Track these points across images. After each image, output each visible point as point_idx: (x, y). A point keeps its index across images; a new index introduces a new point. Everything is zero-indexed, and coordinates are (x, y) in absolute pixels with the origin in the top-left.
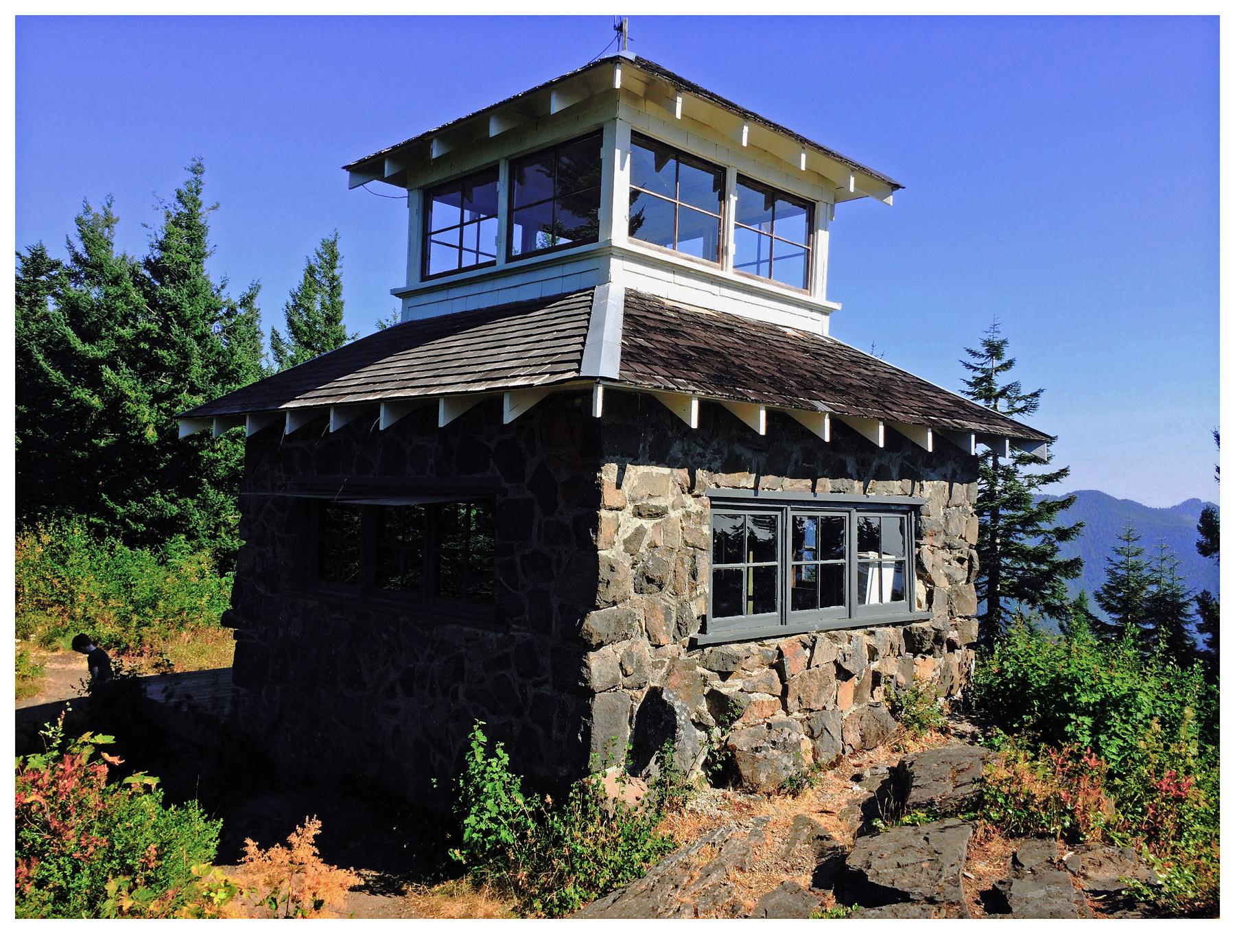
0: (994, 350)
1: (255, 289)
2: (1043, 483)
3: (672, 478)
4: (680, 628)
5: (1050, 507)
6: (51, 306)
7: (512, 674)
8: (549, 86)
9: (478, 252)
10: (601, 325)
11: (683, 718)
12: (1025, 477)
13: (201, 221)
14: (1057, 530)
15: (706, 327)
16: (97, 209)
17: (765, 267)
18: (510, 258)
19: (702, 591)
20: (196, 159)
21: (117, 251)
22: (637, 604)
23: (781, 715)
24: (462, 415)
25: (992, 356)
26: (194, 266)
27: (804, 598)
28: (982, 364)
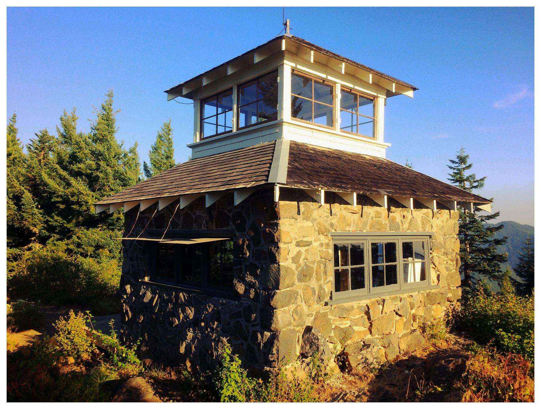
1: (136, 145)
2: (487, 219)
3: (314, 228)
5: (491, 230)
6: (52, 156)
7: (242, 320)
9: (225, 127)
10: (278, 158)
11: (322, 341)
12: (479, 217)
13: (112, 118)
14: (495, 240)
15: (327, 157)
16: (69, 114)
17: (355, 128)
18: (238, 129)
19: (330, 280)
20: (110, 91)
21: (78, 131)
22: (299, 287)
23: (369, 336)
24: (217, 201)
25: (462, 163)
26: (109, 136)
27: (378, 281)
28: (457, 167)
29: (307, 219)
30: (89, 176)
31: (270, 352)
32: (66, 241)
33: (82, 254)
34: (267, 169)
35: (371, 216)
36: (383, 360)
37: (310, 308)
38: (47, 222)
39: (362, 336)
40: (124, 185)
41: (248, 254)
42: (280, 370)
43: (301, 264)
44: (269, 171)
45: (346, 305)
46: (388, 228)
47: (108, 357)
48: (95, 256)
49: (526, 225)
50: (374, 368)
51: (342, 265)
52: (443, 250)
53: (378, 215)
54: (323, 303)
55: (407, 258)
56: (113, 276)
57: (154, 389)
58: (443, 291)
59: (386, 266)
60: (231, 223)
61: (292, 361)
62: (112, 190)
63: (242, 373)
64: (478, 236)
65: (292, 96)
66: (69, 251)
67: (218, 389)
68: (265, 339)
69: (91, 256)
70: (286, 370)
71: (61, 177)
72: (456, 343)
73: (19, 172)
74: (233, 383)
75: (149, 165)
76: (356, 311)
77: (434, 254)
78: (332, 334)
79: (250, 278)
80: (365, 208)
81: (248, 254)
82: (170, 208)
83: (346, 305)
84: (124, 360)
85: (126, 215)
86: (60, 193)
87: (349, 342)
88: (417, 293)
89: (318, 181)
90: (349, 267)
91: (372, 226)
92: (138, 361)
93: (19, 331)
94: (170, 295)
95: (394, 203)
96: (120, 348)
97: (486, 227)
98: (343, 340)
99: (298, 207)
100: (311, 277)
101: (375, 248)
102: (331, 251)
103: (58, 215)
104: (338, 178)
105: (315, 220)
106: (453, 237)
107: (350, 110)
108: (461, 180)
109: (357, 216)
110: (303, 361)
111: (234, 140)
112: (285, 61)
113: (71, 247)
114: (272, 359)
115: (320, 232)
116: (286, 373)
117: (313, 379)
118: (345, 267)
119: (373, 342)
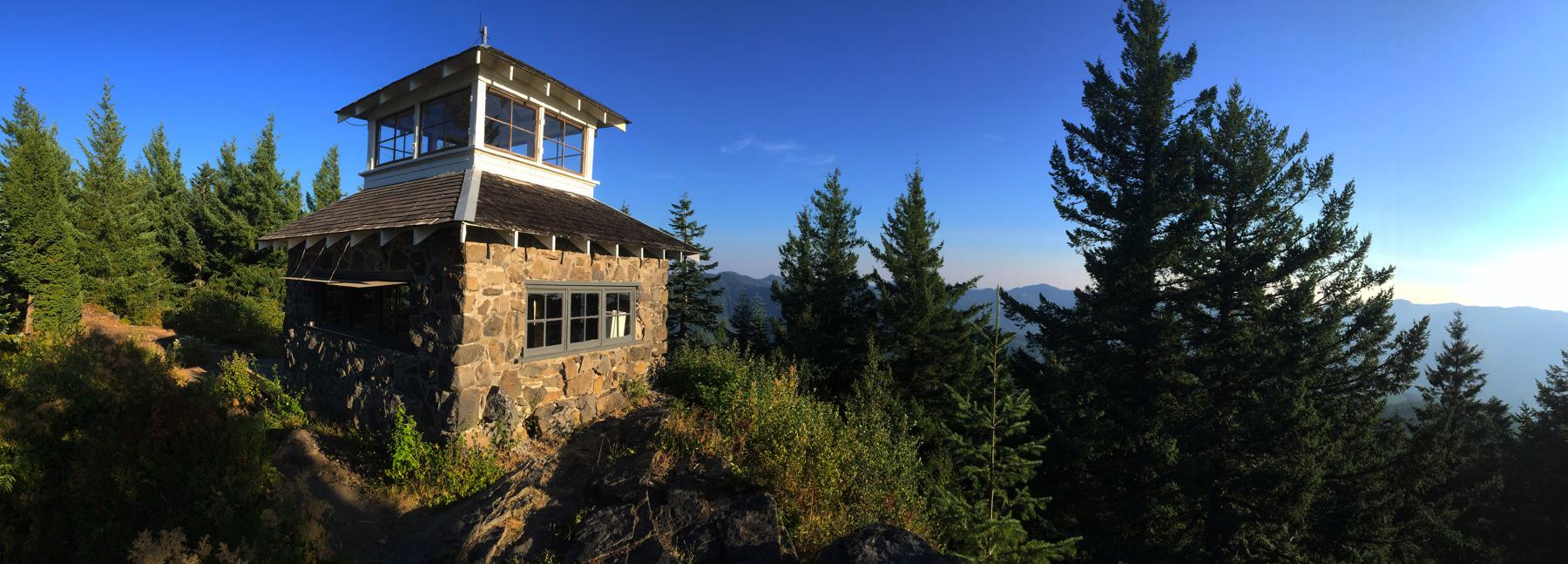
0: (685, 205)
1: (298, 174)
4: (509, 355)
6: (212, 190)
8: (443, 62)
9: (404, 152)
10: (467, 191)
13: (273, 144)
15: (523, 191)
17: (560, 160)
18: (420, 155)
21: (237, 162)
22: (485, 341)
23: (563, 398)
24: (394, 239)
26: (270, 165)
29: (498, 263)
30: (248, 209)
31: (448, 414)
32: (226, 279)
33: (242, 293)
34: (454, 204)
35: (572, 262)
36: (577, 423)
37: (498, 365)
38: (209, 258)
39: (556, 397)
40: (286, 218)
41: (427, 302)
42: (458, 435)
43: (488, 316)
44: (455, 207)
45: (539, 363)
46: (591, 277)
47: (271, 404)
48: (255, 294)
49: (745, 276)
50: (566, 432)
51: (537, 318)
52: (650, 302)
53: (580, 262)
54: (513, 360)
55: (611, 311)
56: (273, 317)
57: (319, 445)
58: (647, 345)
59: (587, 320)
60: (408, 265)
61: (473, 426)
62: (272, 224)
63: (416, 436)
64: (696, 286)
65: (486, 118)
66: (229, 289)
67: (390, 452)
68: (443, 400)
69: (250, 294)
70: (465, 435)
71: (222, 212)
72: (658, 399)
73: (184, 207)
74: (406, 447)
75: (312, 195)
76: (550, 369)
77: (641, 307)
78: (522, 396)
79: (428, 330)
80: (566, 253)
81: (427, 302)
82: (339, 246)
83: (539, 363)
84: (288, 409)
85: (291, 252)
86: (221, 228)
87: (540, 404)
88: (619, 349)
89: (511, 220)
90: (544, 321)
91: (573, 274)
92: (301, 411)
93: (187, 367)
94: (337, 343)
95: (597, 249)
96: (284, 395)
97: (705, 277)
98: (533, 403)
99: (488, 249)
100: (500, 330)
101: (576, 299)
102: (524, 302)
103: (219, 252)
104: (536, 218)
105: (507, 265)
106: (661, 288)
107: (555, 140)
108: (682, 227)
109: (556, 263)
110: (486, 426)
111: (415, 168)
112: (480, 77)
113: (232, 284)
114: (450, 423)
115: (512, 280)
116: (465, 438)
117: (498, 446)
118: (540, 321)
119: (567, 404)
